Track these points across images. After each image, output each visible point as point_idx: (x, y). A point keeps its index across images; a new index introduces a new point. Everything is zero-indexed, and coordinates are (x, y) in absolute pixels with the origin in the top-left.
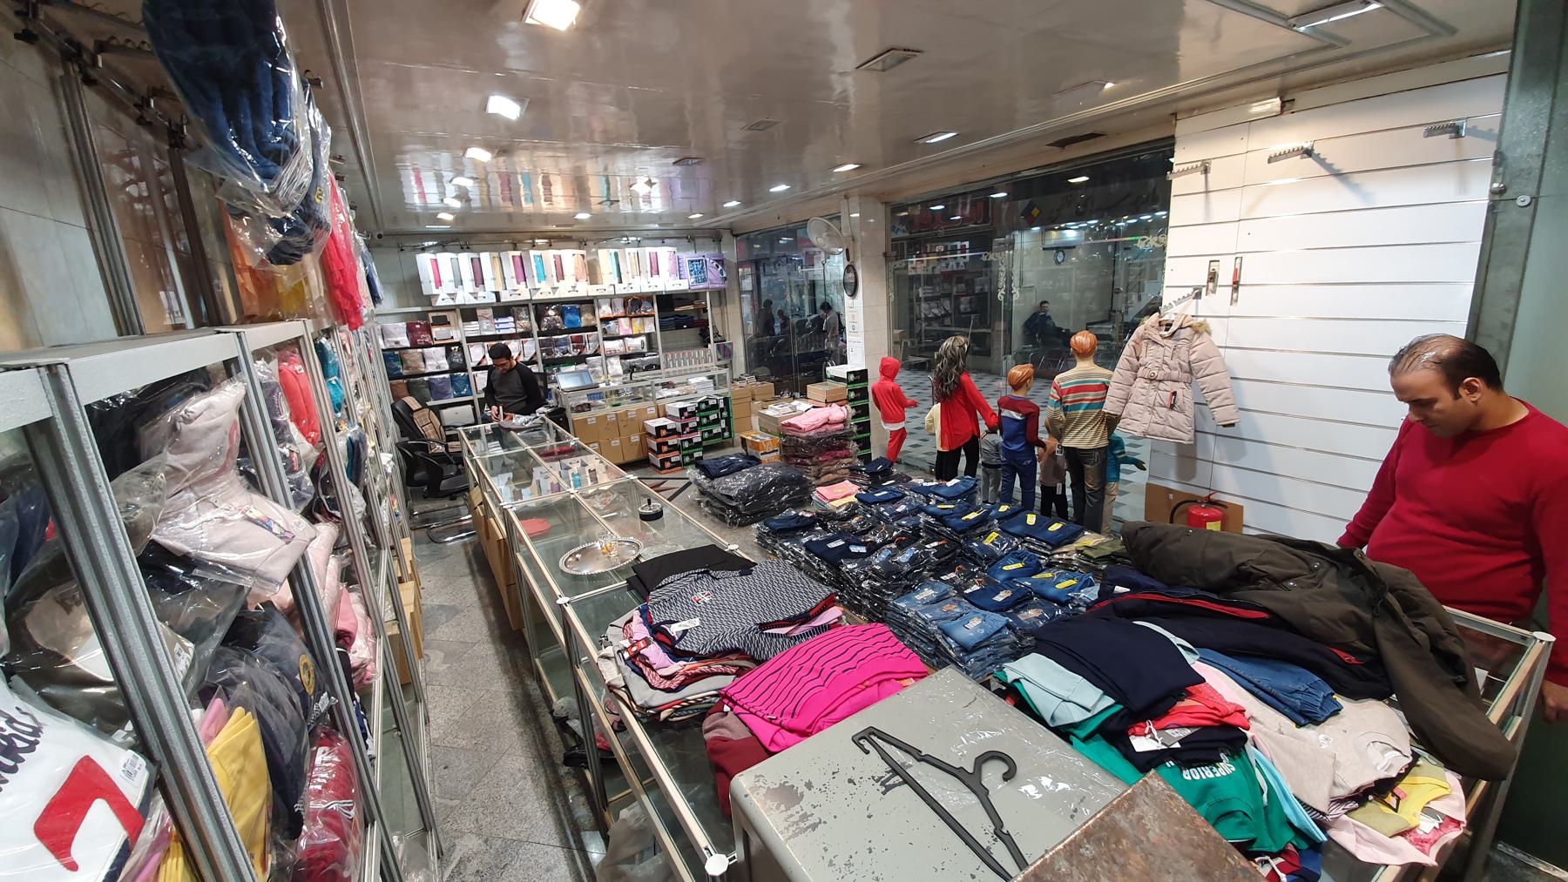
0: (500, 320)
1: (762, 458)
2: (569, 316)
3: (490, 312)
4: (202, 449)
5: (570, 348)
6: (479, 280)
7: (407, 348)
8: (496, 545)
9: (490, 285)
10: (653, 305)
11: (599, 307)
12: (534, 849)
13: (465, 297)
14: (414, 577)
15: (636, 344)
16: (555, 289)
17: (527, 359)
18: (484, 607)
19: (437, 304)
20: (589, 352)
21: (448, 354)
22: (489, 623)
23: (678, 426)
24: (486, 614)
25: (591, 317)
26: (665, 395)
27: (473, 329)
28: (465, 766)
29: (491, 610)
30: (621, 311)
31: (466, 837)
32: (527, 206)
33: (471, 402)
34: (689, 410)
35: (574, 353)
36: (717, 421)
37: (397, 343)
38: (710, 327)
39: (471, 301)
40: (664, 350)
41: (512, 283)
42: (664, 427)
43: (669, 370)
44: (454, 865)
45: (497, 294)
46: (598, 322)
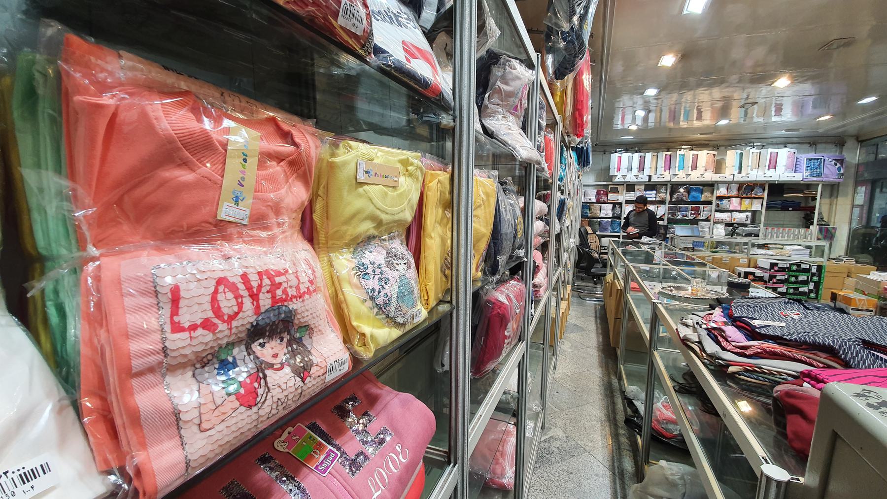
0: (648, 192)
1: (851, 312)
2: (693, 193)
3: (643, 187)
4: (511, 86)
5: (689, 214)
6: (641, 168)
7: (594, 203)
8: (616, 291)
9: (647, 171)
10: (764, 190)
11: (718, 189)
12: (593, 460)
13: (631, 178)
14: (568, 300)
15: (741, 217)
16: (688, 175)
18: (597, 333)
20: (702, 218)
21: (613, 209)
22: (598, 341)
23: (766, 276)
24: (598, 337)
25: (710, 195)
26: (759, 253)
28: (567, 397)
29: (601, 337)
30: (734, 192)
31: (558, 429)
32: (683, 124)
35: (691, 217)
36: (805, 283)
37: (590, 199)
38: (816, 212)
39: (634, 180)
40: (766, 225)
41: (661, 170)
42: (753, 274)
44: (547, 437)
45: (650, 177)
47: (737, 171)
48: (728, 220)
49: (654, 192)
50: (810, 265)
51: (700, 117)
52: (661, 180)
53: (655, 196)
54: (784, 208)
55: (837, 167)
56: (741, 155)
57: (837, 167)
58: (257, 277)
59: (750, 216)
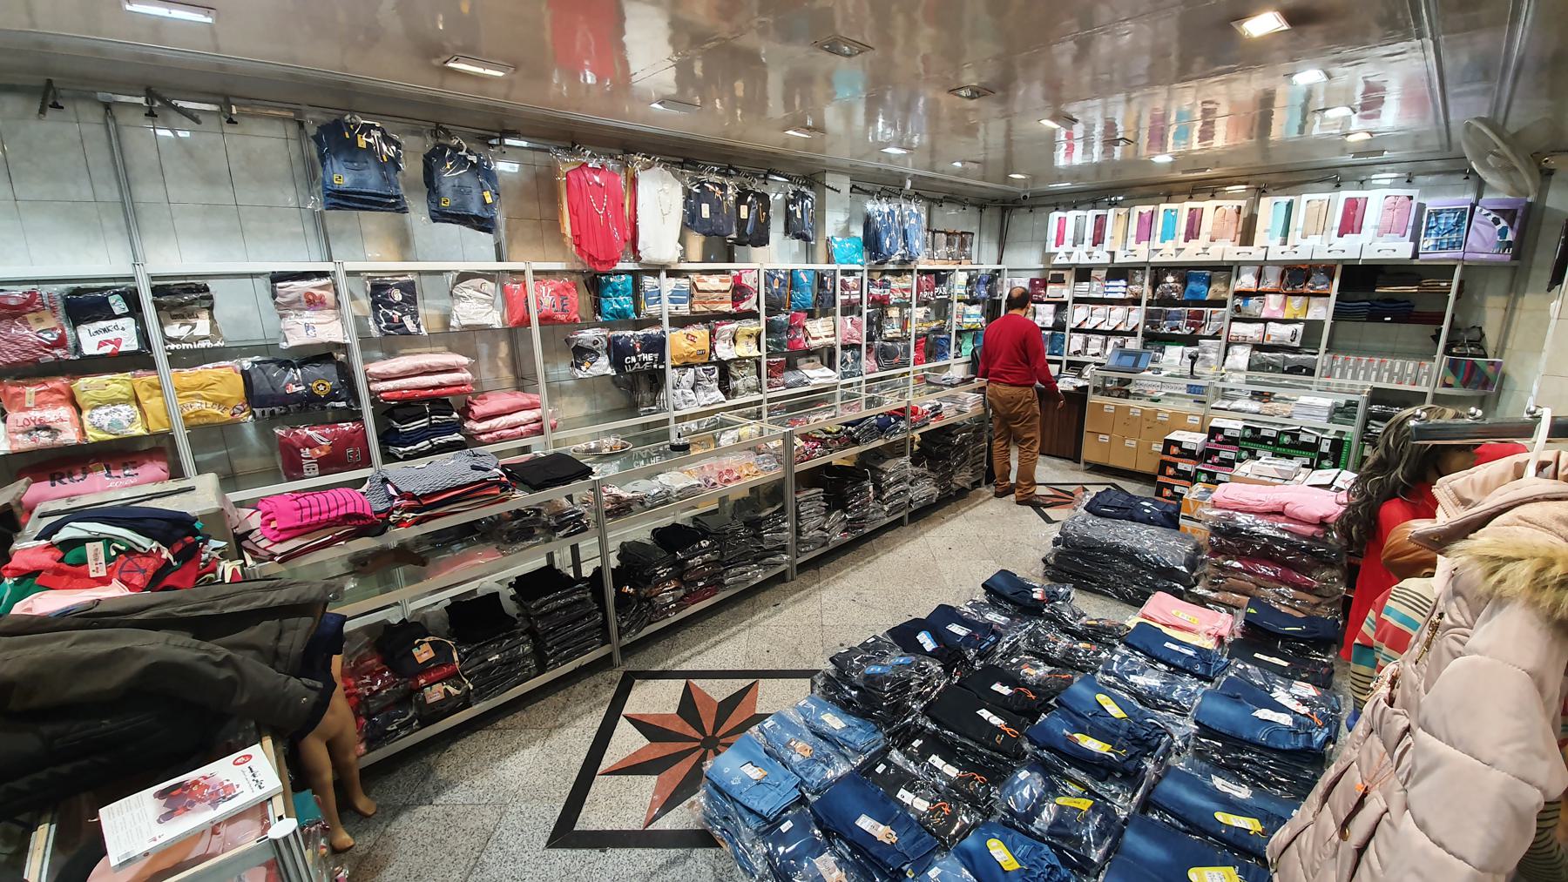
0: (1111, 283)
2: (1192, 285)
6: (1098, 239)
10: (1332, 280)
13: (1080, 256)
15: (1279, 332)
17: (1110, 328)
19: (1055, 262)
20: (1207, 333)
25: (1222, 289)
27: (1083, 289)
30: (1271, 282)
33: (1060, 362)
34: (1227, 433)
35: (1186, 331)
39: (1085, 260)
43: (1330, 380)
45: (1112, 254)
46: (1230, 296)
47: (1279, 239)
48: (1257, 337)
49: (1123, 282)
50: (1318, 438)
51: (1207, 134)
52: (1130, 259)
53: (1124, 290)
54: (1375, 316)
55: (1499, 227)
56: (1290, 205)
57: (1499, 227)
58: (1125, 358)
59: (1300, 332)
